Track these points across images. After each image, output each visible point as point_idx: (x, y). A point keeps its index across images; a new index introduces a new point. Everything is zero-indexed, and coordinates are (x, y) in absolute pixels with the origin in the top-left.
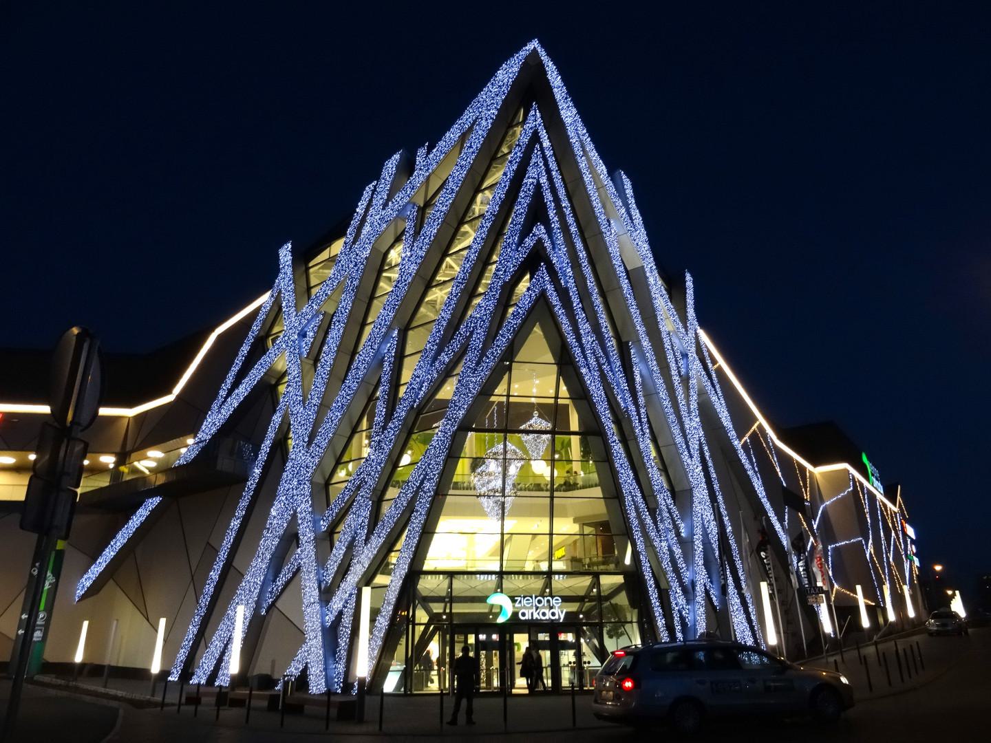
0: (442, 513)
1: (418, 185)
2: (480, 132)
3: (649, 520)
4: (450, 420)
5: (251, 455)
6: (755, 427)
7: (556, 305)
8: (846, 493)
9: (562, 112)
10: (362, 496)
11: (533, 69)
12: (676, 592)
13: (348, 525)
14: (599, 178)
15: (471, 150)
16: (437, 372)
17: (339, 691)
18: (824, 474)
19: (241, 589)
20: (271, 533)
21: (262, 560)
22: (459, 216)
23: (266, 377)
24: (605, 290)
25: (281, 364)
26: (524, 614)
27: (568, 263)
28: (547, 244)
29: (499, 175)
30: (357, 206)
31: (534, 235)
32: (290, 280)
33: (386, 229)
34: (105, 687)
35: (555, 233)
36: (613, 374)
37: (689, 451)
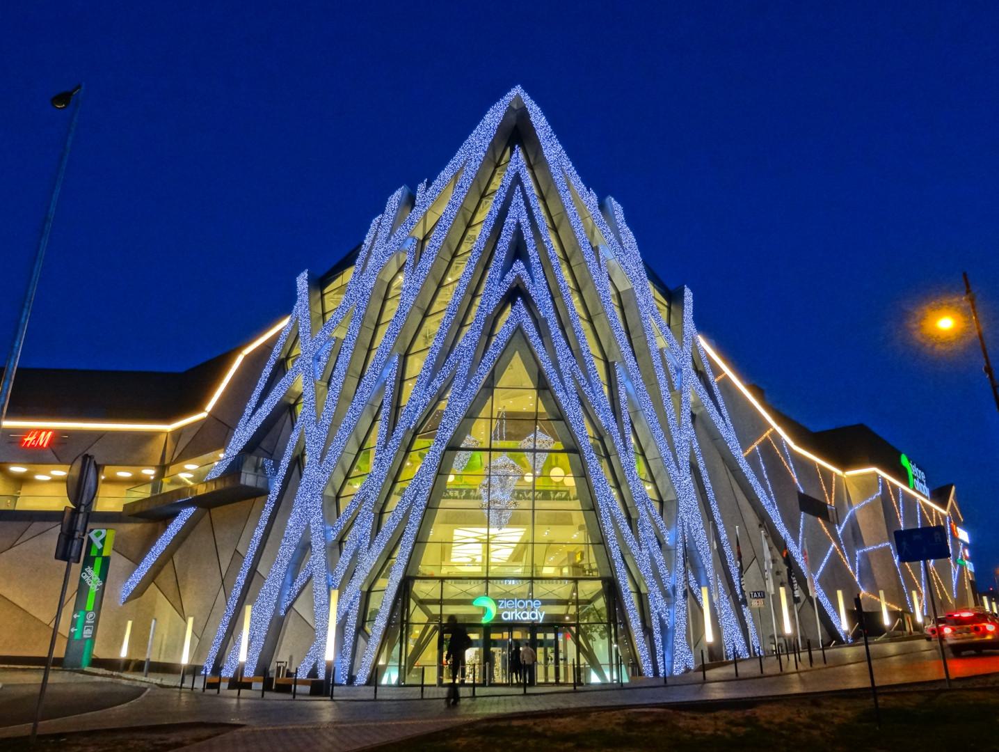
2: (470, 173)
4: (439, 441)
6: (767, 434)
7: (532, 336)
8: (874, 497)
12: (656, 596)
23: (286, 399)
25: (299, 385)
26: (506, 616)
30: (364, 238)
34: (146, 676)
37: (677, 464)
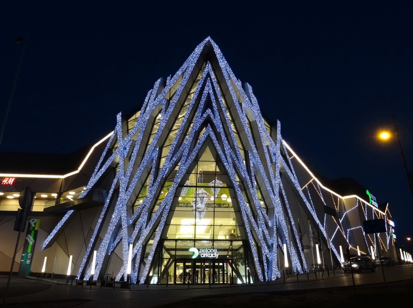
0: (173, 216)
3: (253, 220)
5: (106, 195)
6: (311, 181)
7: (214, 140)
8: (355, 207)
9: (220, 64)
10: (144, 211)
12: (265, 248)
16: (172, 164)
17: (135, 283)
18: (346, 200)
22: (180, 106)
23: (111, 165)
24: (239, 131)
25: (117, 160)
26: (202, 255)
27: (220, 123)
29: (195, 89)
30: (145, 99)
31: (207, 113)
32: (120, 127)
33: (155, 108)
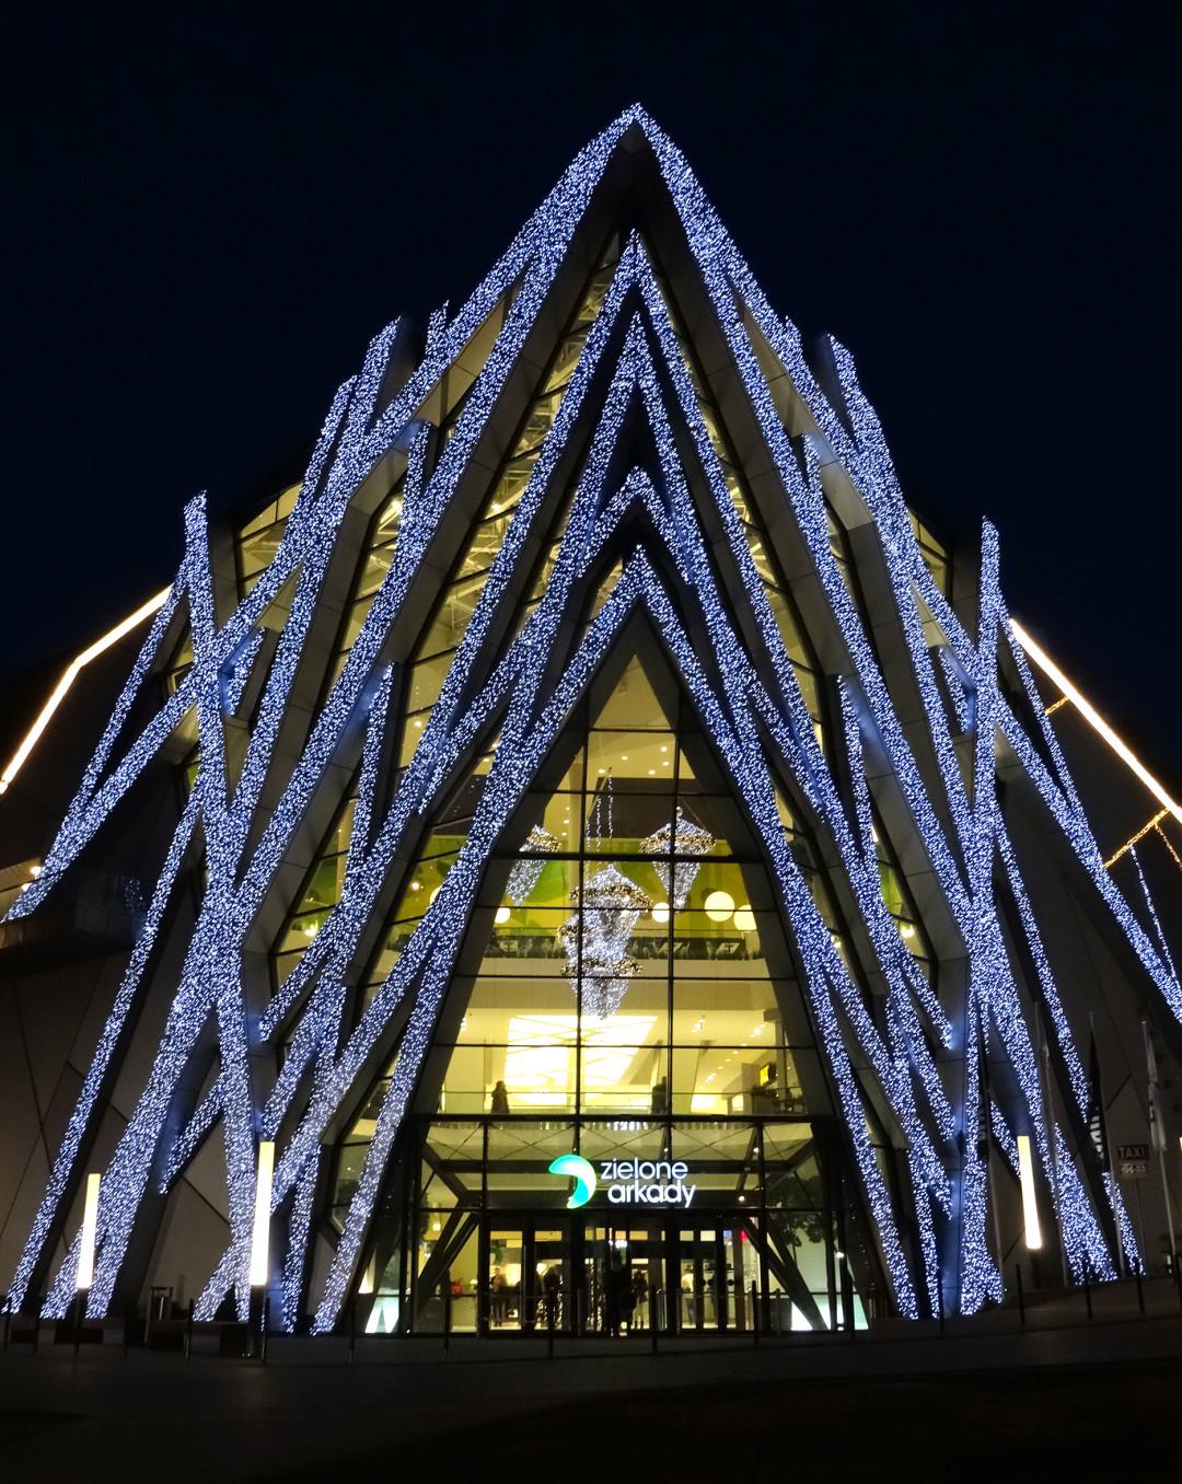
0: (470, 1003)
1: (428, 388)
3: (863, 1019)
10: (329, 978)
11: (634, 163)
12: (923, 1155)
13: (304, 1030)
14: (776, 358)
15: (521, 321)
16: (458, 748)
17: (290, 1330)
19: (123, 1147)
20: (172, 1046)
21: (159, 1094)
24: (789, 577)
26: (617, 1194)
27: (697, 538)
28: (654, 506)
30: (323, 425)
32: (204, 568)
35: (670, 483)
36: (796, 744)
37: (966, 883)
